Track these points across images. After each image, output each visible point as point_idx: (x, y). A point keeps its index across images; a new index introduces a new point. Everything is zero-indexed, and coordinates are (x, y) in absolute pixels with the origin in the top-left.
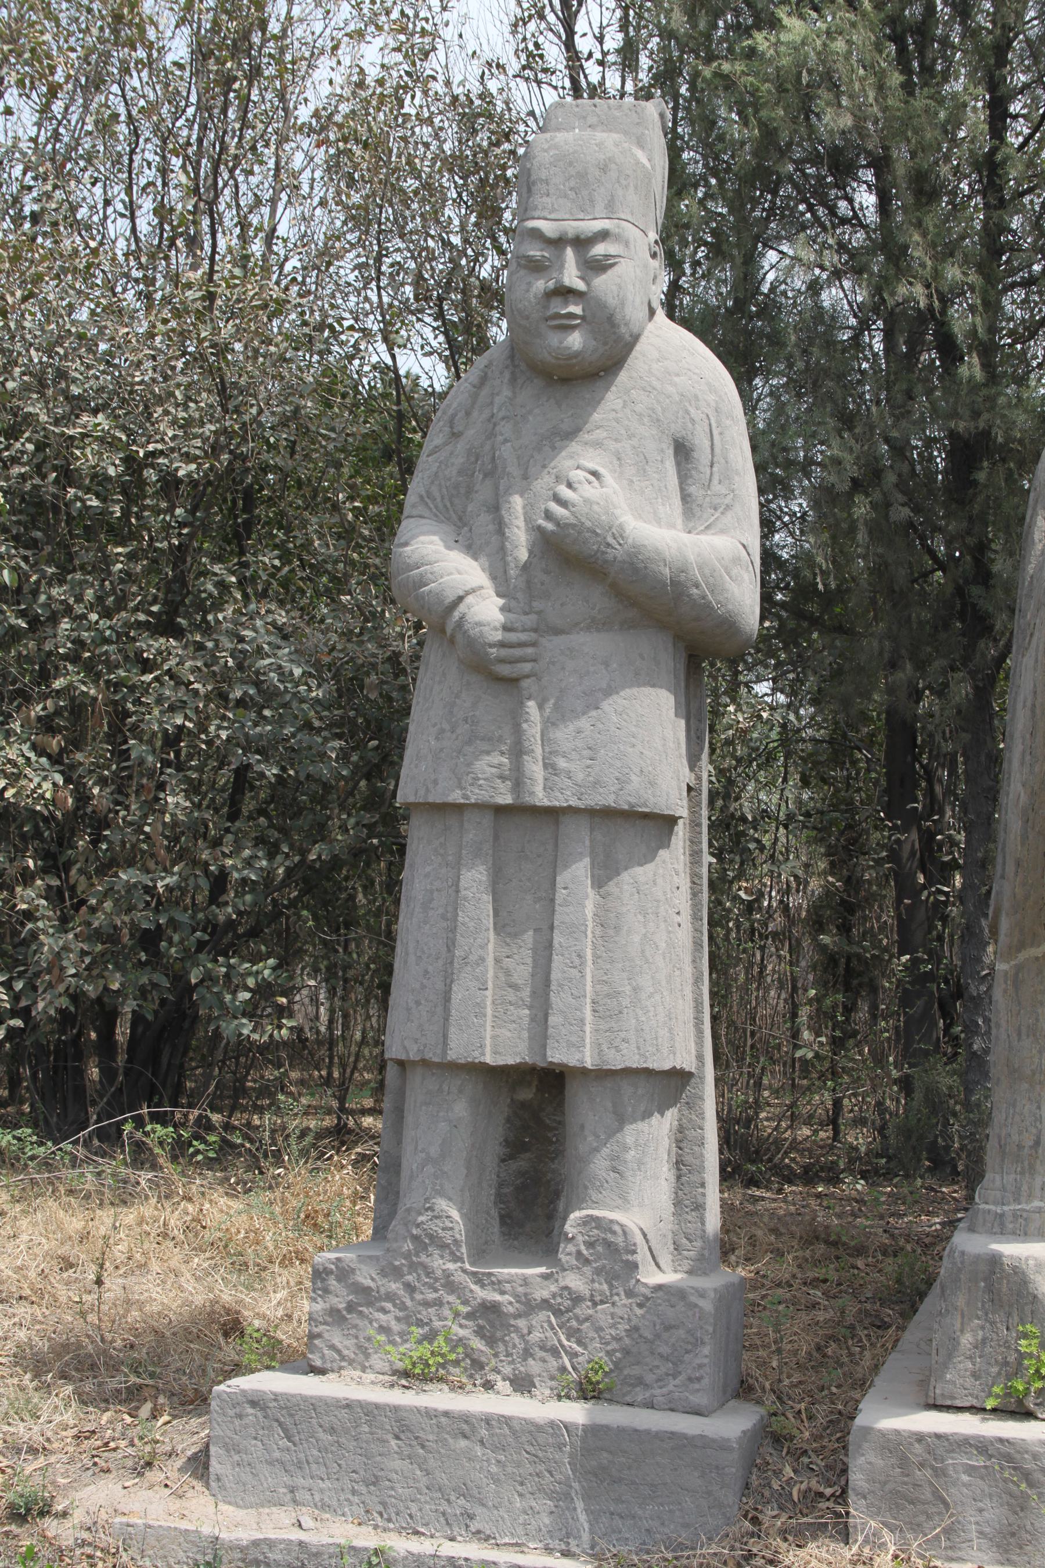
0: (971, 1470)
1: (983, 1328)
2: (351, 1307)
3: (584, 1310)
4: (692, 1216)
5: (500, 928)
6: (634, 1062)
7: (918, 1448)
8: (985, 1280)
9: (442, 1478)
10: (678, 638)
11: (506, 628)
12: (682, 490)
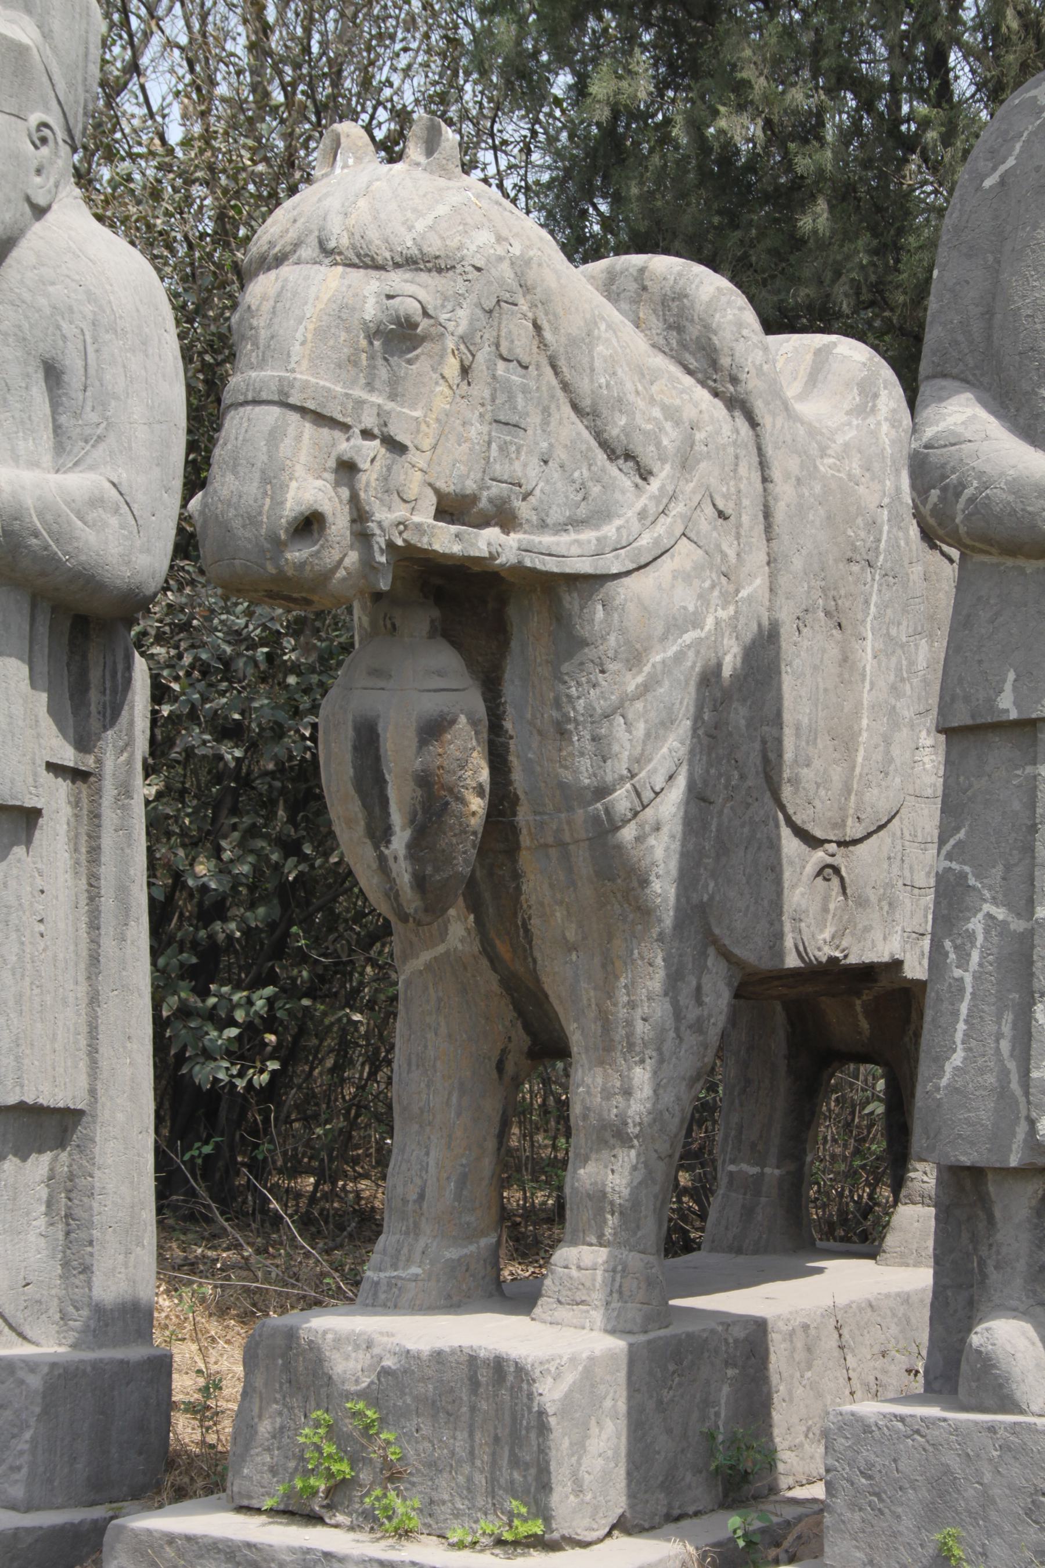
1: (280, 1414)
7: (170, 1552)
8: (283, 1356)
10: (36, 599)
12: (54, 420)
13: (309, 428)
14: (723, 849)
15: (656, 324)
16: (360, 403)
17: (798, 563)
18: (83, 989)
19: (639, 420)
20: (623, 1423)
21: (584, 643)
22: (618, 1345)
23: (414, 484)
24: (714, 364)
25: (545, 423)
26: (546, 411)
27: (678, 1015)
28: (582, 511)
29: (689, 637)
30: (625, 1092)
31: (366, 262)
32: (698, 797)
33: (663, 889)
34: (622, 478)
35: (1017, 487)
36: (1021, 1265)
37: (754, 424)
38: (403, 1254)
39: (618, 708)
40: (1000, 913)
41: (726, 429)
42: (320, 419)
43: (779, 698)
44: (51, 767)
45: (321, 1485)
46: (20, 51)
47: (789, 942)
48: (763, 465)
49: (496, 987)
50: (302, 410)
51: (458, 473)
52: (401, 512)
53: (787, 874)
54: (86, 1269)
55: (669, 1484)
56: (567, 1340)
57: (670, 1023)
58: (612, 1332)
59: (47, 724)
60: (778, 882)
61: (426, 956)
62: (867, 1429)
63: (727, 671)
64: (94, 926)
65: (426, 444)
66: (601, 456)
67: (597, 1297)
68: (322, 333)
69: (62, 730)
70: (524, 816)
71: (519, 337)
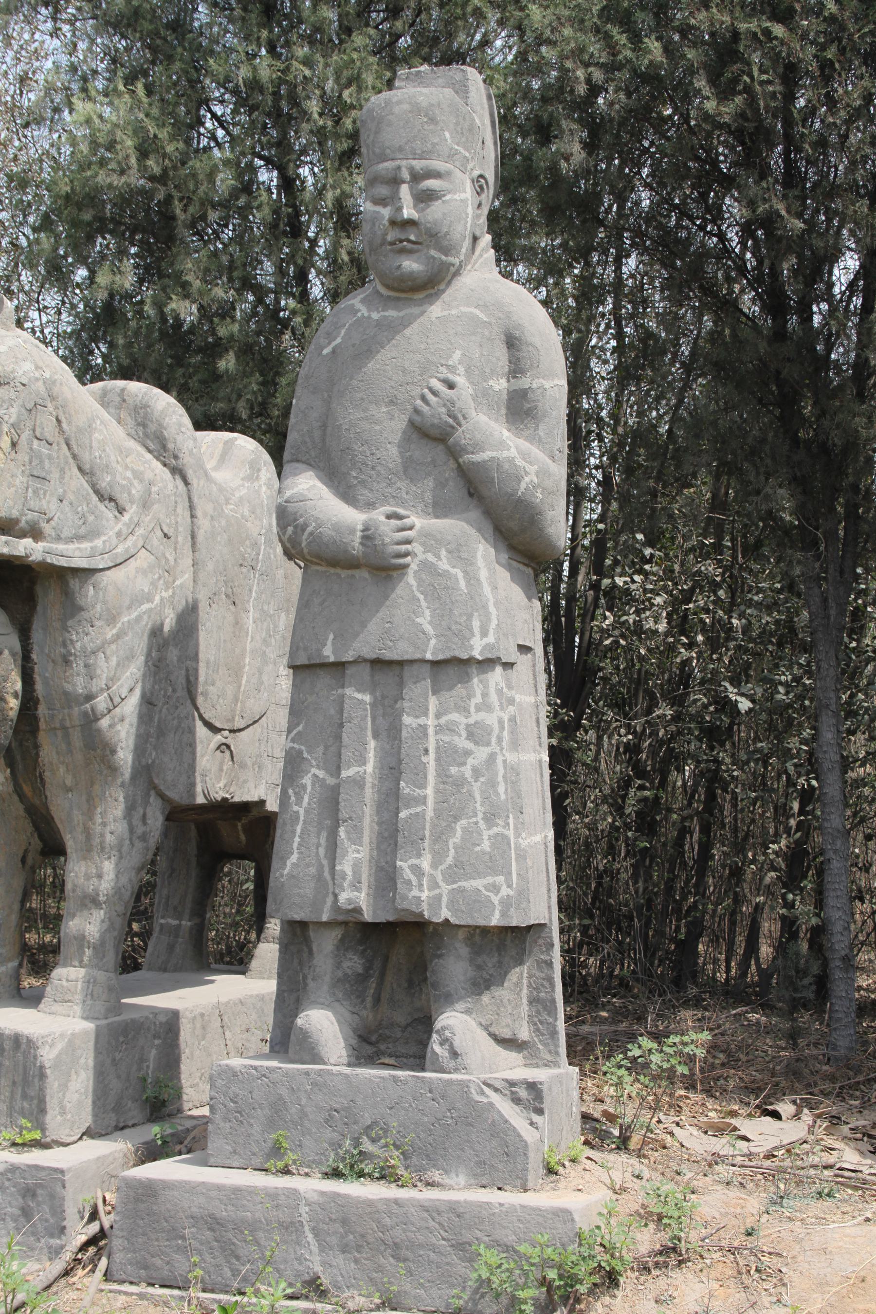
14: (161, 733)
15: (130, 422)
17: (210, 566)
20: (91, 1073)
21: (81, 609)
22: (90, 1026)
24: (164, 447)
25: (62, 477)
26: (62, 471)
27: (132, 830)
28: (83, 531)
29: (145, 607)
32: (148, 702)
33: (125, 756)
34: (107, 512)
36: (327, 978)
37: (186, 483)
39: (101, 648)
40: (321, 774)
41: (170, 486)
43: (197, 645)
47: (199, 789)
48: (191, 507)
53: (199, 749)
57: (126, 835)
58: (86, 1018)
60: (194, 753)
62: (235, 1075)
63: (166, 629)
66: (95, 498)
67: (78, 997)
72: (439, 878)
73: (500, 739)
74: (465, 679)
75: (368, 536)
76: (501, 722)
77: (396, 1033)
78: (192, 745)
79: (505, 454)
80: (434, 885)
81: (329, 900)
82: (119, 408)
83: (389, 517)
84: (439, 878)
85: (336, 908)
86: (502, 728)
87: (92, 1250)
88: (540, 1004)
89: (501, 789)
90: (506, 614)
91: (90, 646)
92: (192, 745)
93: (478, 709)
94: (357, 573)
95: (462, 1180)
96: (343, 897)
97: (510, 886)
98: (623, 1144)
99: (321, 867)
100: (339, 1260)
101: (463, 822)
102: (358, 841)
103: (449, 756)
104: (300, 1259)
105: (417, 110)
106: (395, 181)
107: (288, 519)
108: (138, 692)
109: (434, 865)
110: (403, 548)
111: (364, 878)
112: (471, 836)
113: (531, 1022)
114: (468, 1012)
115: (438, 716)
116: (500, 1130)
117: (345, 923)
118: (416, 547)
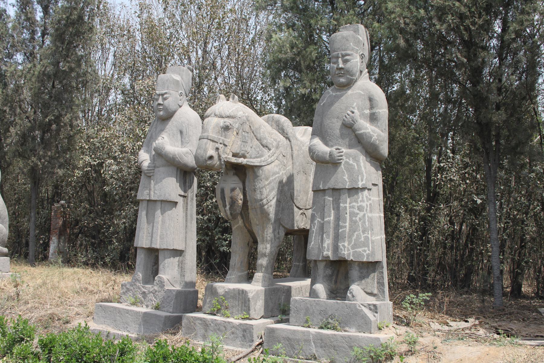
0: (199, 323)
2: (126, 292)
3: (157, 293)
4: (183, 278)
5: (147, 222)
6: (166, 248)
9: (124, 321)
11: (148, 167)
13: (211, 142)
14: (283, 209)
15: (275, 125)
16: (220, 139)
17: (297, 164)
18: (184, 231)
19: (269, 141)
20: (263, 301)
21: (258, 176)
22: (263, 288)
23: (228, 151)
24: (284, 132)
25: (251, 142)
26: (252, 140)
27: (275, 236)
28: (258, 155)
29: (277, 176)
30: (266, 249)
31: (222, 117)
32: (278, 201)
33: (272, 216)
34: (265, 150)
35: (323, 153)
36: (322, 276)
37: (290, 141)
38: (232, 273)
39: (264, 187)
40: (320, 220)
41: (285, 142)
42: (213, 141)
43: (294, 186)
44: (179, 195)
45: (216, 309)
46: (178, 81)
47: (295, 225)
48: (292, 148)
49: (247, 231)
50: (210, 140)
51: (236, 150)
52: (226, 156)
53: (295, 214)
54: (184, 276)
55: (272, 311)
56: (255, 288)
57: (273, 237)
58: (263, 286)
59: (179, 188)
60: (293, 215)
61: (236, 226)
62: (296, 301)
63: (284, 181)
64: (186, 221)
65: (230, 145)
66: (261, 147)
67: (261, 281)
68: (214, 128)
69: (181, 189)
70: (249, 204)
71: (247, 127)
72: (350, 248)
73: (366, 210)
74: (357, 193)
75: (331, 155)
76: (367, 205)
77: (338, 292)
78: (293, 213)
79: (367, 131)
80: (348, 250)
81: (321, 254)
82: (272, 122)
83: (336, 149)
84: (350, 248)
85: (323, 256)
86: (367, 207)
87: (260, 346)
88: (381, 284)
89: (367, 223)
90: (370, 175)
91: (261, 186)
92: (293, 213)
93: (361, 201)
94: (329, 165)
95: (354, 330)
96: (325, 253)
97: (369, 250)
98: (408, 324)
99: (319, 245)
100: (320, 350)
101: (356, 233)
102: (328, 238)
103: (353, 214)
104: (310, 349)
105: (343, 37)
106: (338, 57)
107: (311, 150)
108: (275, 199)
109: (349, 245)
110: (340, 158)
111: (330, 248)
112: (358, 237)
113: (378, 288)
114: (358, 285)
115: (350, 204)
116: (364, 317)
117: (326, 261)
118: (344, 157)
